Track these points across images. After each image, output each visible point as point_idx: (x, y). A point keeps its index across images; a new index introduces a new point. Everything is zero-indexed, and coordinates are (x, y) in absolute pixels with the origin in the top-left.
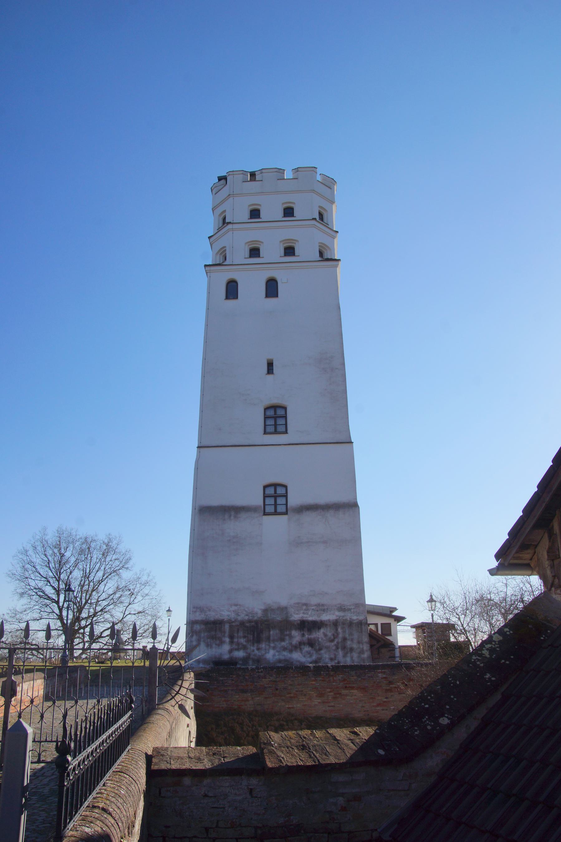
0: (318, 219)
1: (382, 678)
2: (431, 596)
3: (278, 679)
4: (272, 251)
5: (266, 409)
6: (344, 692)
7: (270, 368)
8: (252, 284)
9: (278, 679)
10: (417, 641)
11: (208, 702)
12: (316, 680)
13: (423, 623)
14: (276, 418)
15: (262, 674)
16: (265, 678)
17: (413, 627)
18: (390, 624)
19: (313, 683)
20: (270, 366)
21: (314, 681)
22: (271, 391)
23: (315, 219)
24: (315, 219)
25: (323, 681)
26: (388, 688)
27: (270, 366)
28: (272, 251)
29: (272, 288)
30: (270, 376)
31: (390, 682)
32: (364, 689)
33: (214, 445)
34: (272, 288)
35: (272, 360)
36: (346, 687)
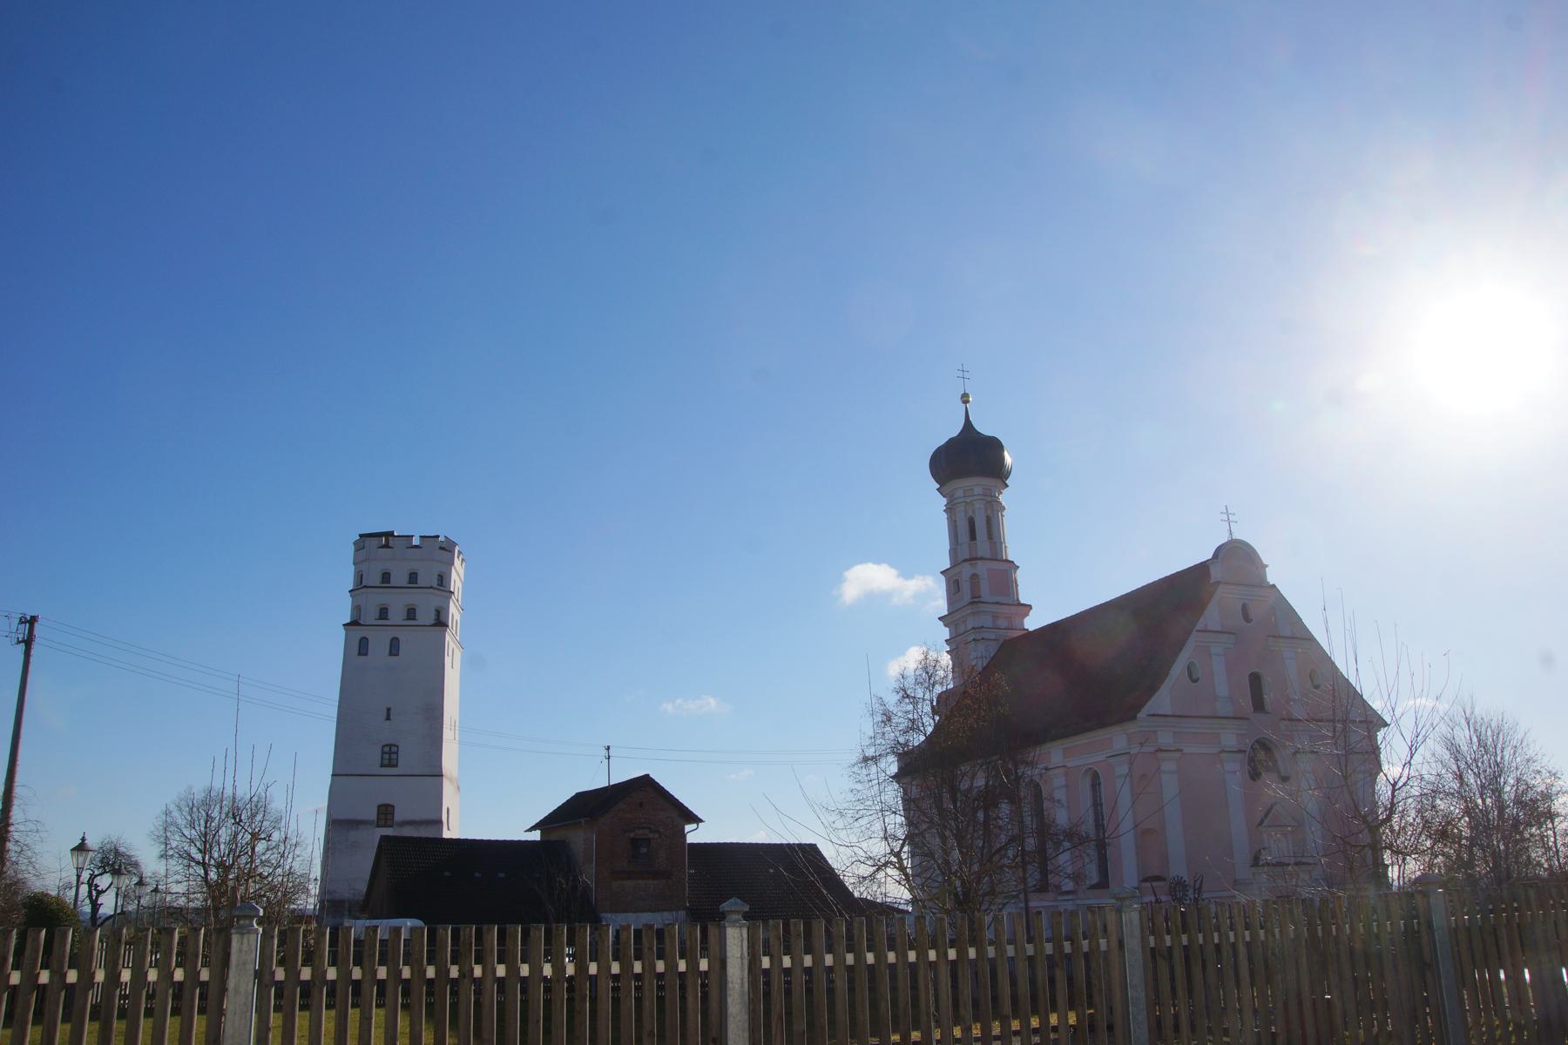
4: (397, 616)
5: (379, 807)
8: (379, 641)
14: (390, 756)
28: (397, 616)
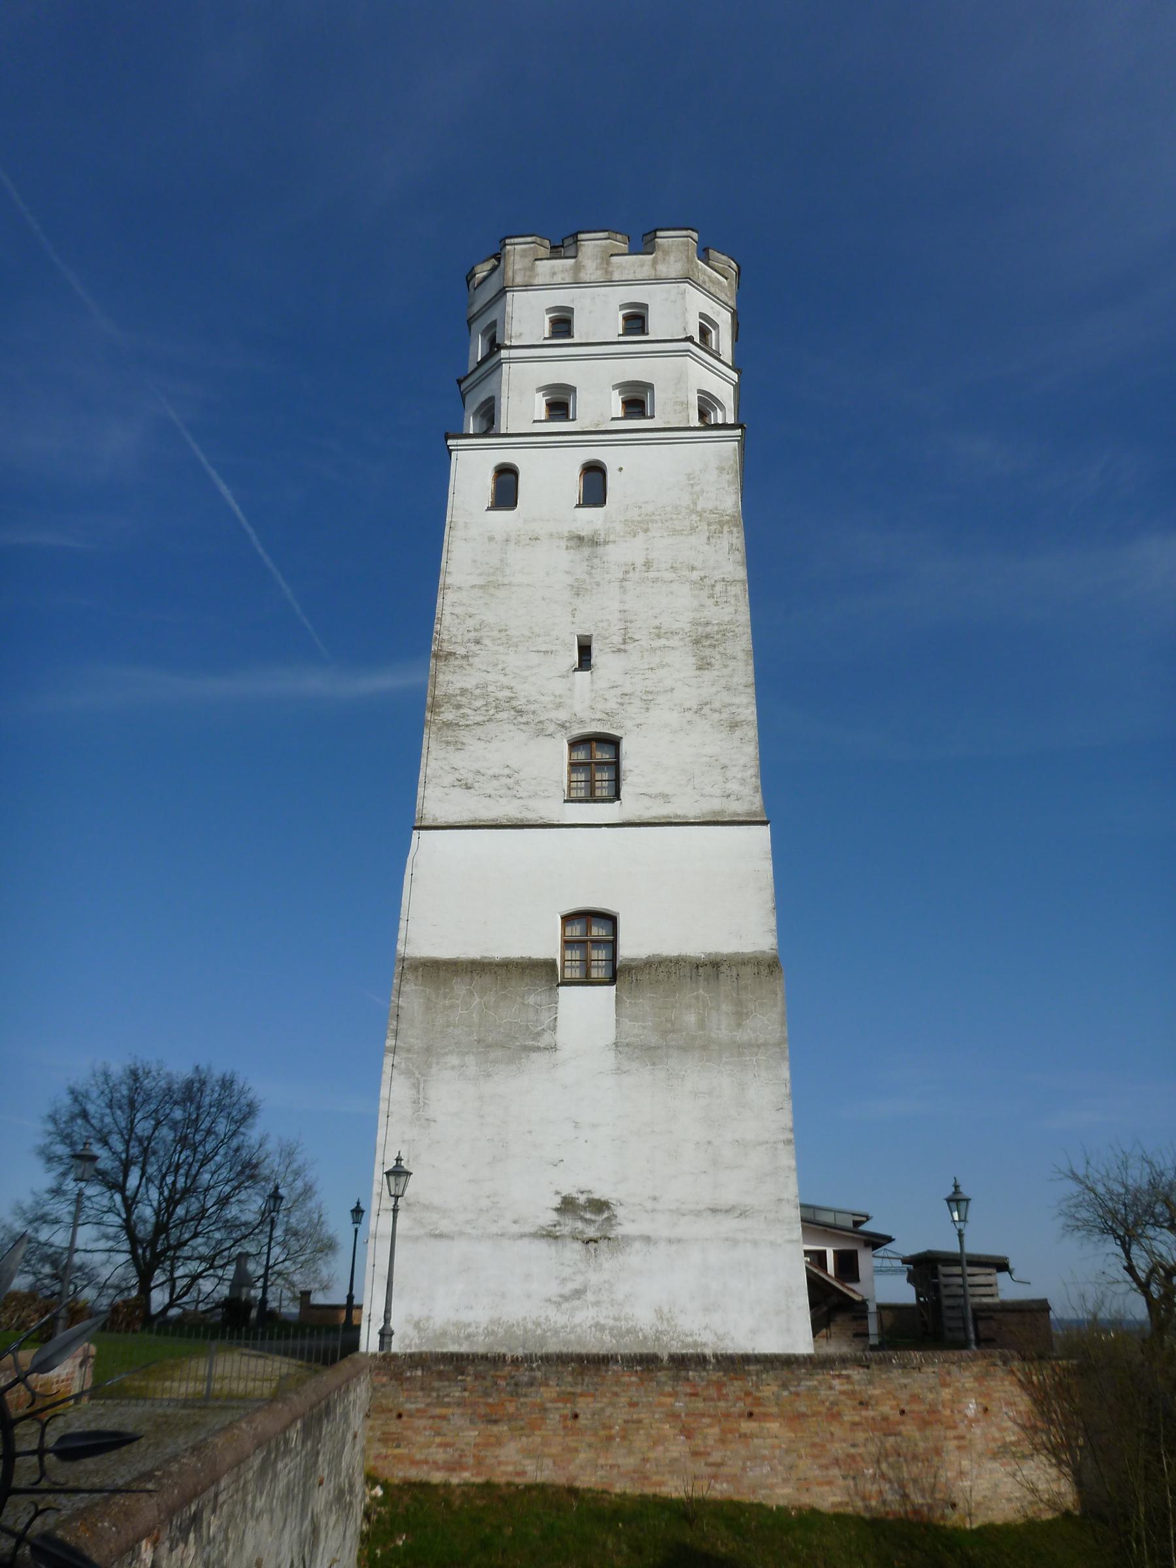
0: (697, 340)
1: (842, 1393)
2: (358, 1203)
3: (579, 1390)
4: (598, 403)
6: (746, 1426)
7: (585, 658)
9: (579, 1390)
10: (918, 1295)
11: (398, 1446)
12: (675, 1394)
13: (929, 1252)
15: (539, 1374)
16: (547, 1385)
17: (905, 1261)
18: (856, 1252)
19: (669, 1400)
20: (585, 650)
21: (670, 1395)
22: (586, 702)
23: (690, 339)
24: (690, 339)
25: (691, 1395)
26: (857, 1419)
27: (585, 650)
28: (598, 403)
29: (595, 480)
30: (585, 674)
31: (861, 1403)
32: (795, 1419)
33: (452, 819)
34: (595, 480)
35: (589, 637)
36: (751, 1414)
